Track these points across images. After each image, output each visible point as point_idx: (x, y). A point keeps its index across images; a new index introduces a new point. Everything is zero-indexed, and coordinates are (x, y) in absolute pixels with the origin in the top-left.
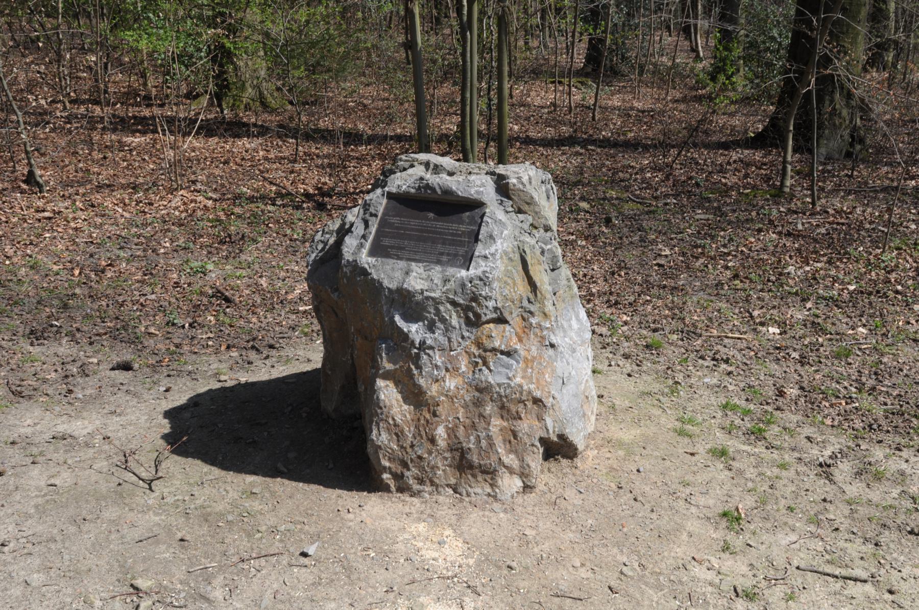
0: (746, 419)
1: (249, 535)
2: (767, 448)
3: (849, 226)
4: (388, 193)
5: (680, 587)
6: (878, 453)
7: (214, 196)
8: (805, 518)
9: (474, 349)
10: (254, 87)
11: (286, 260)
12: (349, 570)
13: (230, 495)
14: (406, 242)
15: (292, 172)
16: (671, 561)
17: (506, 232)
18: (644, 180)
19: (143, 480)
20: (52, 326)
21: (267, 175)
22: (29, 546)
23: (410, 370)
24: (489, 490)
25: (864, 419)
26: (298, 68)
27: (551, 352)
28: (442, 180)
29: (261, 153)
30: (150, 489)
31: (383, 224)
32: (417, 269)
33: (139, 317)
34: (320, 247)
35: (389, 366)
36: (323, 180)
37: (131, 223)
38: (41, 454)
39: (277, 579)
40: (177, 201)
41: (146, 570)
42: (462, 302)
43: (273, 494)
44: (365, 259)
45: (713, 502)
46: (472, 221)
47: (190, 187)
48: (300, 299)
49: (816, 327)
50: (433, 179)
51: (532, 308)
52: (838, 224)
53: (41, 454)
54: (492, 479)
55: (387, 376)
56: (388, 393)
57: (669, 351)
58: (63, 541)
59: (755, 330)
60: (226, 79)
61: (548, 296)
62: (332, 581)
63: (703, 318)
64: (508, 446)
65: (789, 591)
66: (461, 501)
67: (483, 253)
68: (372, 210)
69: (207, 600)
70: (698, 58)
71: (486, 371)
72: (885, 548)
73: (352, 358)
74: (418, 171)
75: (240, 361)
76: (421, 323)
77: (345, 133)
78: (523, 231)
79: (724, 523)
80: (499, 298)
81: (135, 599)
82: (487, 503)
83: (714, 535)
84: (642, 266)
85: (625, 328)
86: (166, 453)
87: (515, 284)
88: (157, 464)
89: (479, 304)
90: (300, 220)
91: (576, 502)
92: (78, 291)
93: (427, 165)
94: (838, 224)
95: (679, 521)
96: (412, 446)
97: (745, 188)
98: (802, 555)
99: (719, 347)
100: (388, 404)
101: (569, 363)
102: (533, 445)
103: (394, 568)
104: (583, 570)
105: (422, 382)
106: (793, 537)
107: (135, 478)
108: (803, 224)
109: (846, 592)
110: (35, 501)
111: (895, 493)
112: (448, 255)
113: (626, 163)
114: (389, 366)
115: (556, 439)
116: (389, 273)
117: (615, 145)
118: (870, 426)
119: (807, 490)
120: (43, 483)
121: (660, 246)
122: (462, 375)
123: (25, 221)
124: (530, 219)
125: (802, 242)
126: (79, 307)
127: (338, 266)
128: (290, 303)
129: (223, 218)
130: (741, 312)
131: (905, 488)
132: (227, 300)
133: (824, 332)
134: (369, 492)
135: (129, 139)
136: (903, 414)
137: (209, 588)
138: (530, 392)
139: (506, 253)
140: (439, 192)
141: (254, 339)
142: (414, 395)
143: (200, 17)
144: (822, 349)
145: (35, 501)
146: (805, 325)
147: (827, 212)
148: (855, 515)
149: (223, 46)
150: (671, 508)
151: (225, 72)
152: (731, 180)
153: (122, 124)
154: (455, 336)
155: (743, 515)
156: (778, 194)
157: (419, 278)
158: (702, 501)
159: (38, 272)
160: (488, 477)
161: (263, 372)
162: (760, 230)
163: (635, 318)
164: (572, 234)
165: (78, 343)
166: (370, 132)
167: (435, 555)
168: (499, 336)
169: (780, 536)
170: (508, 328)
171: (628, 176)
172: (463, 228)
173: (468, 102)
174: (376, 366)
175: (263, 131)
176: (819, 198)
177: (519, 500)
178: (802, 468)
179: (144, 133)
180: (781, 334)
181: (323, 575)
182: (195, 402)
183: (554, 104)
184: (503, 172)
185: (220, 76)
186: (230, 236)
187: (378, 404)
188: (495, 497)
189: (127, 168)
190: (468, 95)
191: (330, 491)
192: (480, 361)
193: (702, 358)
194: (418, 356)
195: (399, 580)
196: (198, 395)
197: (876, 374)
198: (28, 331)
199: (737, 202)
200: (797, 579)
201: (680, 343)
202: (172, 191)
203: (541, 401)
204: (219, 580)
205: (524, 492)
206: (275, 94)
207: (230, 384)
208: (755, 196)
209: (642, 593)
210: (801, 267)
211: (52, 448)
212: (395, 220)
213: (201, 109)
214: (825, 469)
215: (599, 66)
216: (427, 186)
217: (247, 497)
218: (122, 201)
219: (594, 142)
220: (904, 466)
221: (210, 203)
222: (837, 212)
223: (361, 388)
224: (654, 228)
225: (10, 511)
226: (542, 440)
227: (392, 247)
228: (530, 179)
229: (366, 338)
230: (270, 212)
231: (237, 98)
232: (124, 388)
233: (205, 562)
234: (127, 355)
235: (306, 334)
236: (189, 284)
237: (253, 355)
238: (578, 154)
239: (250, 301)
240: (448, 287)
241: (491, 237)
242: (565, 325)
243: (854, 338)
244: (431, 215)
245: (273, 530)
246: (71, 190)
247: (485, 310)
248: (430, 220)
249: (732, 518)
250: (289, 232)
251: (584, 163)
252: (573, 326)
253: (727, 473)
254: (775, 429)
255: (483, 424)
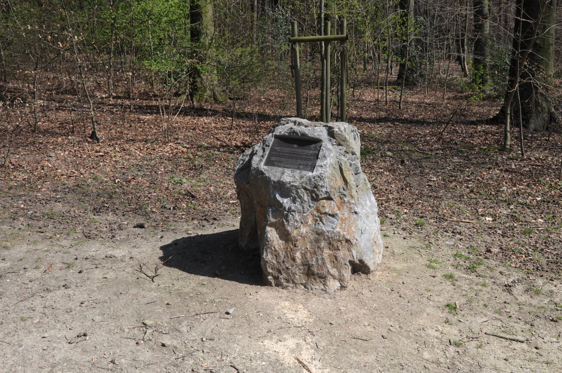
0: (467, 262)
1: (201, 303)
2: (477, 276)
3: (543, 167)
4: (275, 135)
5: (420, 338)
6: (540, 282)
7: (187, 146)
8: (493, 311)
9: (315, 213)
10: (211, 90)
11: (224, 178)
12: (249, 321)
13: (192, 285)
14: (283, 159)
15: (229, 134)
16: (417, 326)
17: (332, 154)
18: (426, 141)
19: (149, 277)
20: (104, 206)
21: (216, 136)
22: (94, 304)
23: (283, 222)
24: (322, 287)
25: (535, 265)
26: (235, 79)
27: (355, 216)
28: (302, 129)
29: (213, 125)
30: (153, 281)
31: (272, 150)
32: (288, 172)
33: (148, 204)
34: (241, 162)
35: (272, 220)
36: (246, 139)
37: (143, 159)
38: (100, 264)
39: (213, 324)
40: (167, 149)
41: (150, 317)
42: (309, 188)
43: (213, 285)
44: (263, 167)
45: (443, 300)
46: (315, 149)
47: (174, 141)
48: (231, 197)
49: (514, 218)
50: (296, 128)
51: (345, 193)
52: (536, 165)
53: (100, 264)
54: (324, 281)
55: (272, 225)
56: (272, 234)
57: (428, 227)
58: (110, 303)
59: (478, 218)
60: (196, 86)
61: (353, 187)
62: (241, 326)
63: (450, 212)
64: (332, 264)
65: (479, 344)
66: (308, 292)
67: (320, 164)
68: (267, 143)
69: (179, 331)
70: (466, 76)
71: (321, 224)
72: (536, 327)
73: (255, 218)
74: (291, 125)
75: (198, 225)
76: (289, 199)
77: (259, 114)
78: (341, 154)
79: (447, 310)
80: (328, 187)
81: (144, 329)
82: (321, 294)
83: (441, 315)
84: (419, 185)
85: (405, 216)
86: (161, 265)
87: (336, 180)
88: (156, 270)
89: (318, 190)
90: (233, 159)
91: (368, 296)
92: (117, 190)
93: (295, 122)
94: (536, 165)
95: (423, 308)
96: (283, 262)
97: (484, 145)
98: (489, 328)
99: (457, 226)
100: (272, 239)
101: (364, 223)
102: (345, 264)
103: (272, 321)
104: (369, 327)
105: (289, 228)
106: (485, 319)
107: (145, 276)
108: (515, 165)
109: (511, 347)
110: (97, 285)
111: (546, 301)
112: (303, 165)
113: (416, 131)
114: (272, 220)
115: (358, 262)
116: (274, 174)
117: (411, 122)
118: (537, 268)
119: (496, 297)
120: (101, 277)
121: (431, 176)
122: (309, 226)
123: (90, 157)
124: (345, 148)
125: (514, 175)
126: (118, 198)
127: (250, 170)
128: (225, 199)
129: (192, 157)
130: (472, 210)
131: (552, 299)
132: (193, 197)
133: (518, 220)
134: (261, 286)
135: (141, 117)
136: (557, 263)
137: (180, 326)
138: (344, 236)
139: (331, 164)
140: (300, 135)
141: (206, 215)
142: (285, 236)
143: (184, 53)
144: (515, 229)
145: (97, 285)
146: (507, 217)
147: (531, 159)
148: (522, 311)
149: (196, 68)
150: (419, 301)
151: (196, 82)
152: (477, 141)
153: (141, 109)
154: (306, 206)
155: (458, 307)
156: (503, 149)
157: (289, 176)
158: (436, 299)
159: (97, 181)
160: (322, 280)
161: (210, 230)
162: (490, 168)
163: (411, 211)
164: (382, 169)
165: (117, 215)
166: (272, 114)
167: (294, 316)
168: (328, 207)
169: (478, 318)
170: (333, 202)
171: (417, 139)
172: (311, 152)
173: (325, 97)
174: (266, 220)
175: (215, 113)
176: (526, 151)
177: (338, 293)
178: (495, 287)
179: (151, 114)
180: (493, 221)
181: (236, 323)
182: (176, 243)
183: (377, 100)
184: (331, 126)
185: (193, 84)
186: (195, 166)
187: (266, 239)
188: (325, 291)
189: (142, 131)
190: (325, 93)
191: (242, 284)
192: (318, 219)
193: (446, 231)
194: (287, 215)
195: (274, 327)
196: (177, 240)
197: (545, 243)
198: (92, 209)
199: (478, 153)
200: (485, 339)
201: (435, 224)
202: (165, 143)
203: (349, 241)
204: (185, 323)
205: (341, 289)
206: (222, 94)
207: (193, 235)
208: (489, 150)
209: (400, 340)
210: (511, 188)
211: (105, 261)
212: (278, 148)
213: (182, 101)
214: (508, 288)
215: (406, 80)
216: (294, 132)
217: (200, 286)
218: (139, 148)
219: (398, 120)
220: (553, 288)
221: (185, 150)
222: (536, 159)
223: (259, 233)
224: (428, 166)
225: (85, 289)
226: (350, 262)
227: (276, 161)
228: (345, 129)
229: (262, 206)
230: (216, 155)
231: (201, 96)
232: (140, 236)
233: (178, 315)
234: (141, 221)
235: (233, 214)
236: (173, 189)
237: (205, 223)
238: (389, 127)
239: (205, 198)
240: (303, 180)
241: (325, 156)
242: (363, 203)
243: (535, 225)
244: (296, 146)
245: (213, 302)
246: (113, 142)
247: (321, 193)
248: (295, 148)
249: (452, 308)
250: (226, 165)
251: (392, 132)
252: (368, 204)
253: (452, 286)
254: (483, 267)
255: (320, 252)
